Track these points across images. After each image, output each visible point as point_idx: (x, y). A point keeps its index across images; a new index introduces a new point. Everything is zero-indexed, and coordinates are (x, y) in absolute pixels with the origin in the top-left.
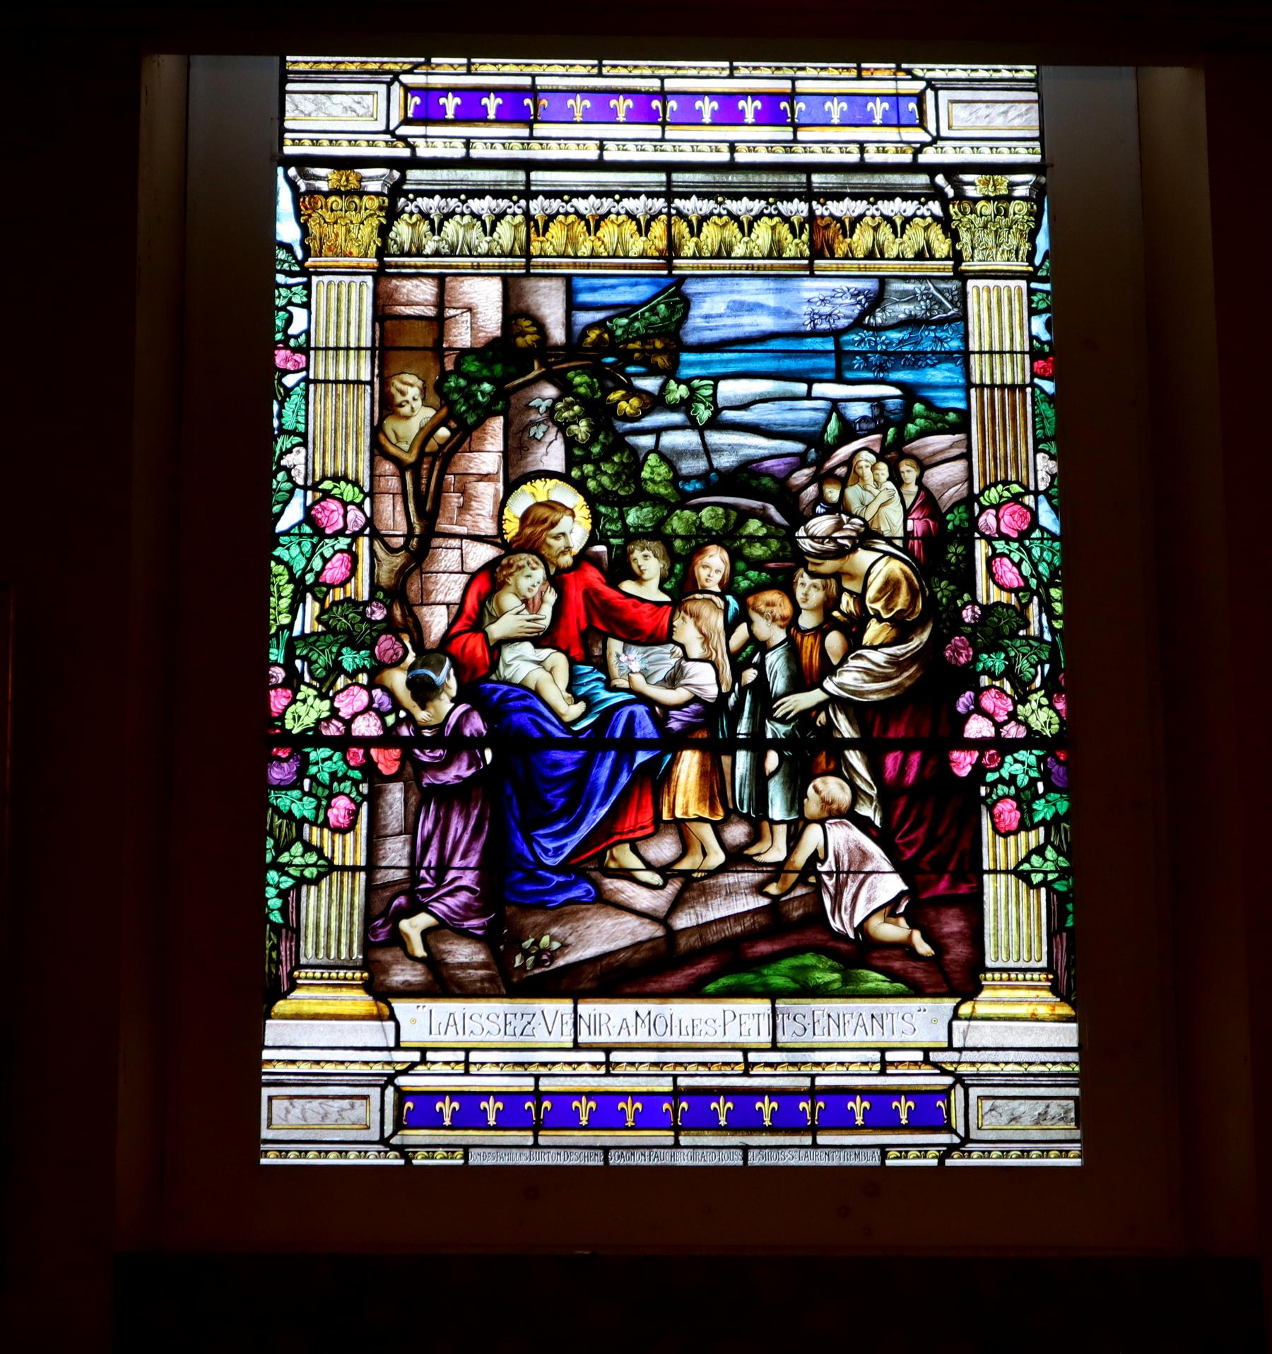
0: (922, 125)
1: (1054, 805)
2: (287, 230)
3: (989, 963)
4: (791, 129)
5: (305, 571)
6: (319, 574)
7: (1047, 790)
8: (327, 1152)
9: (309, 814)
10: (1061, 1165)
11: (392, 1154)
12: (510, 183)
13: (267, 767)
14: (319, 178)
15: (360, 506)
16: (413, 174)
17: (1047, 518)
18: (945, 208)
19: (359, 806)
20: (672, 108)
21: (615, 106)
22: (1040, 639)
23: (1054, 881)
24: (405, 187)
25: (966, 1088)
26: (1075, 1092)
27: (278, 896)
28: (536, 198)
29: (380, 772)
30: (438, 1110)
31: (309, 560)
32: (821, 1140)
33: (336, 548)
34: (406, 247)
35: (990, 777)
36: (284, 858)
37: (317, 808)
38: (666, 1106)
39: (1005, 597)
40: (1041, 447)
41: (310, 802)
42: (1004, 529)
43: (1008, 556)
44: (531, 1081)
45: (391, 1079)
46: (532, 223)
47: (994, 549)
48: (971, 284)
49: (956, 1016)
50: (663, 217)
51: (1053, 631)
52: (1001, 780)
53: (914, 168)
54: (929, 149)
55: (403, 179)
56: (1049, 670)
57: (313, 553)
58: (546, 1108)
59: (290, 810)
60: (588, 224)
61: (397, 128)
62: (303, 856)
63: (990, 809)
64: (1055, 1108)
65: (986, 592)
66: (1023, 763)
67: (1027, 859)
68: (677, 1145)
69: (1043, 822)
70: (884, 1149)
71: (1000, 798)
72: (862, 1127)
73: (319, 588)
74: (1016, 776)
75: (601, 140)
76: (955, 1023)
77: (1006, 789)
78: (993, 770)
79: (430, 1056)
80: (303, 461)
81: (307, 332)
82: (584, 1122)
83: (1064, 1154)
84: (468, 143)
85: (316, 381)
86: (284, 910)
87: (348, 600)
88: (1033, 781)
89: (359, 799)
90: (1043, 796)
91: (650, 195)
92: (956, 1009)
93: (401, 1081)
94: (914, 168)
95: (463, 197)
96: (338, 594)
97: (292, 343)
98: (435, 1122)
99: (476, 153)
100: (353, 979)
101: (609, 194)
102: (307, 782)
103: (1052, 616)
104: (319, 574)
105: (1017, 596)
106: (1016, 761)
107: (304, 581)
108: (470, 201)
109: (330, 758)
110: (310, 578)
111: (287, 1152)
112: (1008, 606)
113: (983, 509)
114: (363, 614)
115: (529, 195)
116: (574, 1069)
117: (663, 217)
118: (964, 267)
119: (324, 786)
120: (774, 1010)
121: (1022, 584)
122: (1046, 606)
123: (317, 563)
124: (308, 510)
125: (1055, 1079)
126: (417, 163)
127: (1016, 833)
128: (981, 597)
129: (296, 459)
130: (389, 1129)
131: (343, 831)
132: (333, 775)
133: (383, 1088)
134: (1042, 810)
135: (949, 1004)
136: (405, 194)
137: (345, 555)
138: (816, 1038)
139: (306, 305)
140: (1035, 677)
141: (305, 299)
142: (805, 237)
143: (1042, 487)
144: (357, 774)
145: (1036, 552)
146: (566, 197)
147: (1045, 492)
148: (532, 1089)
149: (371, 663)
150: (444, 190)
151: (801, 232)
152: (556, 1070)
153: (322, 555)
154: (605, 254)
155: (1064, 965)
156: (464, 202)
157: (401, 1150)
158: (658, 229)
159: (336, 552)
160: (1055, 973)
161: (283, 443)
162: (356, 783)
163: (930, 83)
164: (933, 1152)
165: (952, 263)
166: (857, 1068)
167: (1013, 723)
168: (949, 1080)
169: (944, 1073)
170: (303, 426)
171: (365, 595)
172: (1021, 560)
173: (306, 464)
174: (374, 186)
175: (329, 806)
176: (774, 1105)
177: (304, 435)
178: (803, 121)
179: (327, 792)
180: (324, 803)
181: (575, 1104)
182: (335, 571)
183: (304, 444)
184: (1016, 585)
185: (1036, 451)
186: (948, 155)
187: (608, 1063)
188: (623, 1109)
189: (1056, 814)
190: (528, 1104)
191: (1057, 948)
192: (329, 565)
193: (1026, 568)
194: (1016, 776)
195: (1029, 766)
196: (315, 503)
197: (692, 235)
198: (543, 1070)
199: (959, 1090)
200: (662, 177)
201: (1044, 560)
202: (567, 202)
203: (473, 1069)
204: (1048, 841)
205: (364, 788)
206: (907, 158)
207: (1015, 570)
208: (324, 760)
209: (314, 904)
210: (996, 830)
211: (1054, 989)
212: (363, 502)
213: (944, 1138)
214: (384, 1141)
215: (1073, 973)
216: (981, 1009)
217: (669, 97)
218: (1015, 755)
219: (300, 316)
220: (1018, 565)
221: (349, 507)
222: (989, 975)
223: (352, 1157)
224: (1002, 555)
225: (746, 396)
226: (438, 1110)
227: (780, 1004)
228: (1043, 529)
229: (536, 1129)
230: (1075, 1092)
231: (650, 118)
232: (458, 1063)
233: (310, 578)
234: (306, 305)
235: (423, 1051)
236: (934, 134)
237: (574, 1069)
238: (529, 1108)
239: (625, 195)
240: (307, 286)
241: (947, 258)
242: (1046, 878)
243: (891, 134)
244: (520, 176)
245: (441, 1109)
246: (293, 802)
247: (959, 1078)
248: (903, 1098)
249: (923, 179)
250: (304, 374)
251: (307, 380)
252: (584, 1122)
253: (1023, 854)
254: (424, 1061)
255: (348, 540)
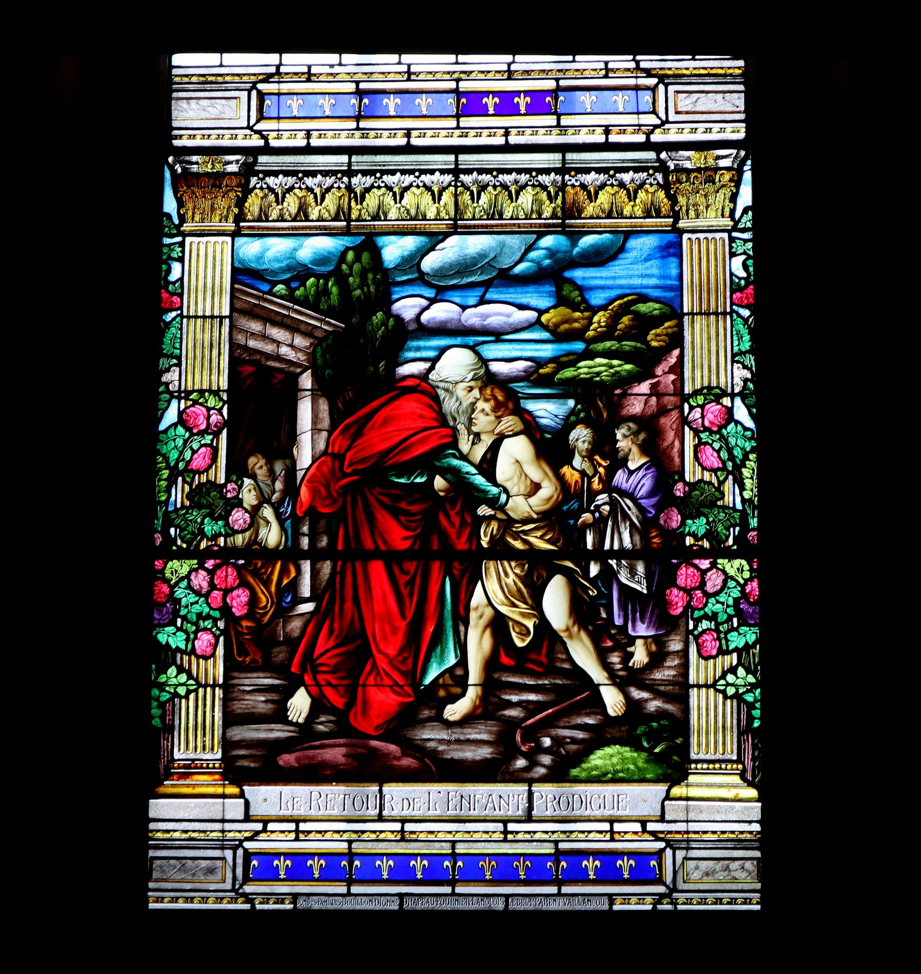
0: (654, 112)
1: (745, 636)
2: (170, 205)
3: (693, 756)
4: (555, 117)
5: (178, 461)
6: (188, 463)
7: (739, 625)
8: (222, 899)
9: (182, 646)
10: (162, 908)
11: (240, 900)
12: (336, 164)
13: (667, 609)
14: (193, 163)
15: (220, 411)
16: (262, 159)
17: (741, 413)
18: (666, 178)
19: (217, 639)
20: (365, 103)
21: (518, 102)
22: (734, 508)
23: (744, 693)
24: (256, 168)
25: (666, 85)
26: (757, 854)
27: (158, 707)
28: (628, 173)
29: (233, 614)
30: (275, 865)
31: (181, 453)
32: (459, 890)
33: (203, 442)
34: (413, 212)
35: (697, 614)
36: (163, 679)
37: (187, 640)
38: (447, 863)
39: (707, 476)
40: (736, 359)
41: (182, 636)
42: (707, 424)
43: (711, 445)
44: (345, 845)
45: (241, 841)
46: (352, 195)
47: (700, 439)
48: (685, 236)
49: (668, 797)
50: (452, 189)
51: (743, 501)
52: (706, 617)
53: (647, 146)
54: (658, 131)
55: (255, 162)
56: (739, 532)
57: (185, 447)
58: (254, 865)
59: (167, 642)
60: (394, 194)
61: (658, 117)
62: (176, 677)
63: (696, 638)
64: (748, 865)
65: (692, 473)
66: (723, 604)
67: (723, 677)
68: (349, 894)
69: (736, 649)
70: (611, 898)
71: (704, 631)
72: (284, 880)
73: (190, 472)
74: (717, 613)
75: (607, 127)
76: (667, 803)
77: (708, 623)
78: (700, 609)
79: (271, 826)
80: (177, 378)
81: (181, 279)
82: (316, 876)
83: (746, 901)
84: (408, 133)
85: (189, 317)
86: (162, 717)
87: (208, 481)
88: (730, 618)
89: (218, 633)
90: (736, 630)
91: (443, 172)
92: (668, 791)
93: (247, 845)
94: (647, 146)
95: (495, 173)
96: (204, 479)
97: (171, 288)
98: (272, 876)
99: (513, 139)
100: (708, 769)
101: (488, 171)
102: (179, 621)
103: (742, 488)
104: (188, 463)
105: (716, 475)
106: (718, 602)
107: (178, 467)
108: (267, 179)
109: (197, 602)
110: (181, 465)
111: (208, 898)
112: (710, 483)
113: (692, 408)
114: (221, 492)
115: (350, 173)
116: (568, 837)
117: (452, 189)
118: (682, 224)
119: (193, 624)
120: (381, 791)
121: (721, 465)
122: (739, 482)
123: (188, 455)
124: (180, 413)
125: (739, 843)
126: (267, 150)
127: (715, 657)
128: (688, 477)
129: (172, 377)
130: (253, 120)
131: (206, 658)
132: (199, 615)
133: (249, 91)
134: (736, 641)
135: (662, 788)
136: (256, 173)
137: (209, 449)
138: (472, 812)
139: (181, 260)
140: (727, 537)
141: (180, 255)
142: (559, 201)
143: (737, 390)
144: (216, 614)
145: (732, 441)
146: (573, 173)
147: (740, 394)
148: (347, 851)
149: (225, 530)
150: (403, 170)
151: (556, 199)
152: (364, 837)
153: (191, 448)
154: (330, 218)
155: (750, 757)
156: (301, 179)
157: (248, 898)
158: (447, 197)
159: (202, 446)
160: (743, 764)
161: (163, 363)
162: (215, 620)
163: (662, 79)
164: (649, 899)
165: (672, 220)
166: (443, 836)
167: (714, 570)
168: (662, 845)
169: (658, 839)
170: (179, 351)
171: (222, 480)
172: (721, 447)
173: (180, 380)
174: (233, 168)
175: (196, 638)
176: (597, 863)
177: (179, 358)
178: (563, 112)
179: (194, 628)
180: (192, 636)
181: (378, 863)
182: (199, 462)
183: (179, 365)
184: (716, 465)
185: (733, 362)
186: (673, 135)
187: (402, 831)
188: (379, 865)
189: (747, 643)
190: (344, 863)
191: (744, 743)
192: (196, 456)
193: (724, 455)
194: (717, 613)
195: (728, 606)
196: (187, 408)
197: (630, 201)
198: (354, 836)
199: (669, 852)
200: (558, 156)
201: (738, 446)
202: (534, 177)
203: (302, 836)
204: (739, 663)
205: (221, 624)
206: (641, 138)
207: (715, 454)
208: (192, 604)
209: (187, 712)
210: (700, 655)
211: (742, 776)
212: (222, 408)
213: (661, 889)
214: (249, 127)
215: (757, 764)
216: (693, 792)
217: (266, 97)
218: (717, 598)
219: (176, 267)
220: (718, 452)
221: (212, 412)
222: (693, 766)
223: (287, 902)
224: (706, 443)
225: (521, 322)
226: (275, 865)
227: (536, 788)
228: (737, 423)
229: (350, 882)
230: (757, 854)
231: (544, 110)
232: (290, 832)
233: (181, 465)
234: (181, 260)
235: (265, 822)
236: (664, 118)
237: (306, 836)
238: (345, 865)
239: (384, 172)
240: (182, 244)
241: (668, 217)
242: (737, 690)
243: (632, 119)
244: (344, 159)
245: (586, 866)
246: (169, 636)
247: (669, 843)
248: (282, 857)
249: (652, 155)
250: (179, 312)
251: (181, 316)
252: (316, 876)
253: (719, 673)
254: (265, 830)
255: (211, 437)
